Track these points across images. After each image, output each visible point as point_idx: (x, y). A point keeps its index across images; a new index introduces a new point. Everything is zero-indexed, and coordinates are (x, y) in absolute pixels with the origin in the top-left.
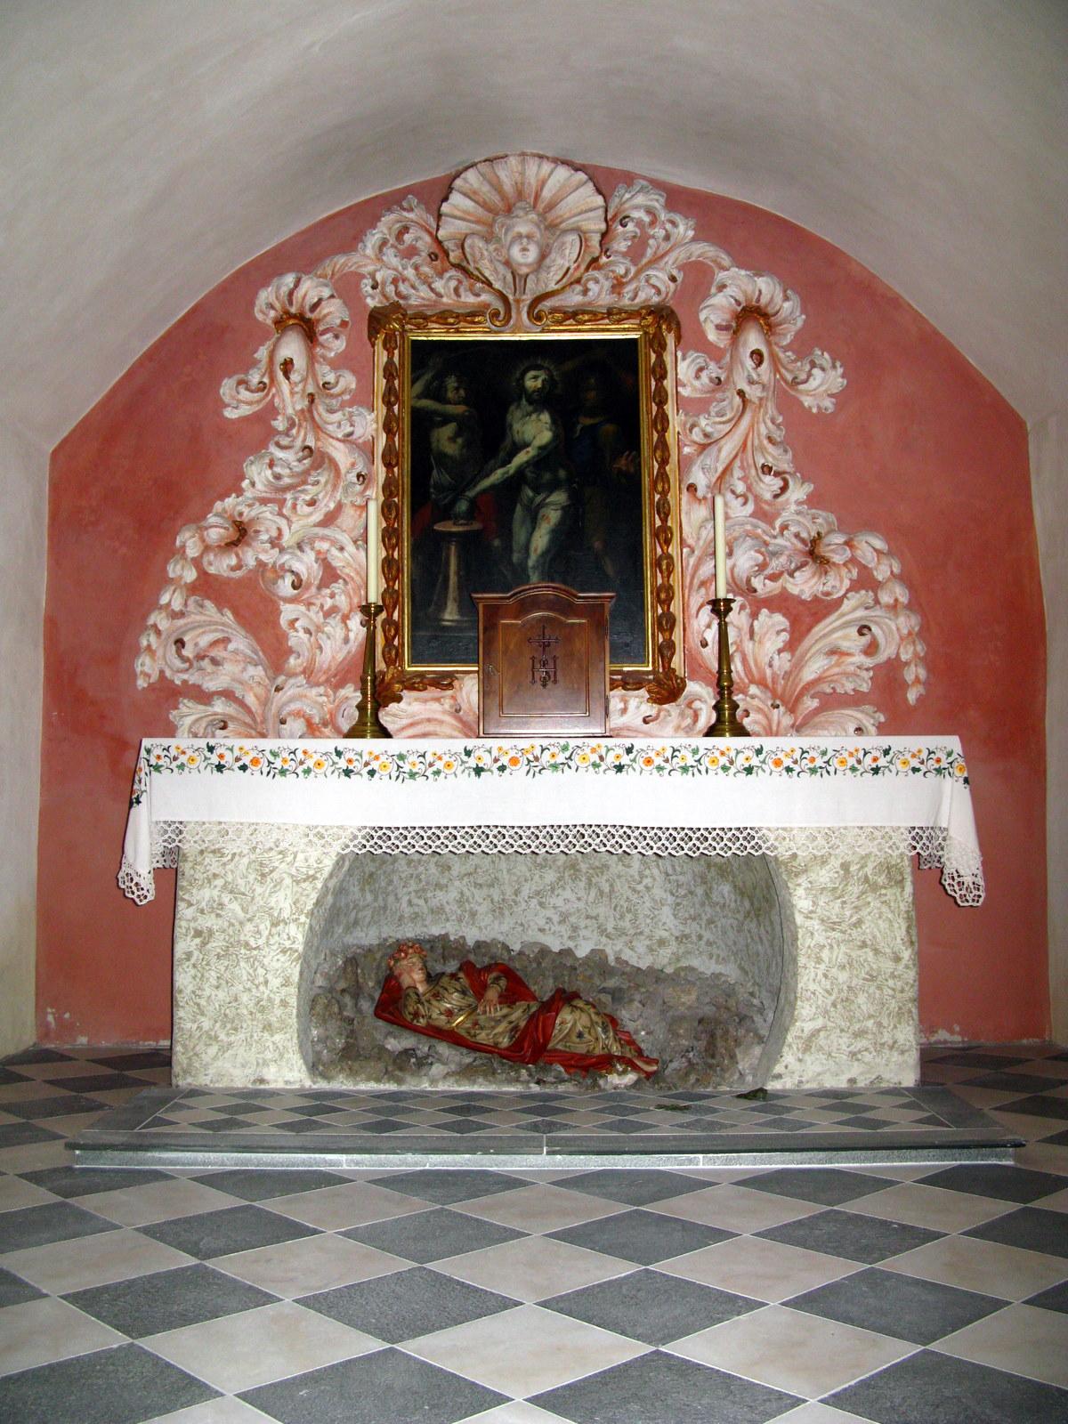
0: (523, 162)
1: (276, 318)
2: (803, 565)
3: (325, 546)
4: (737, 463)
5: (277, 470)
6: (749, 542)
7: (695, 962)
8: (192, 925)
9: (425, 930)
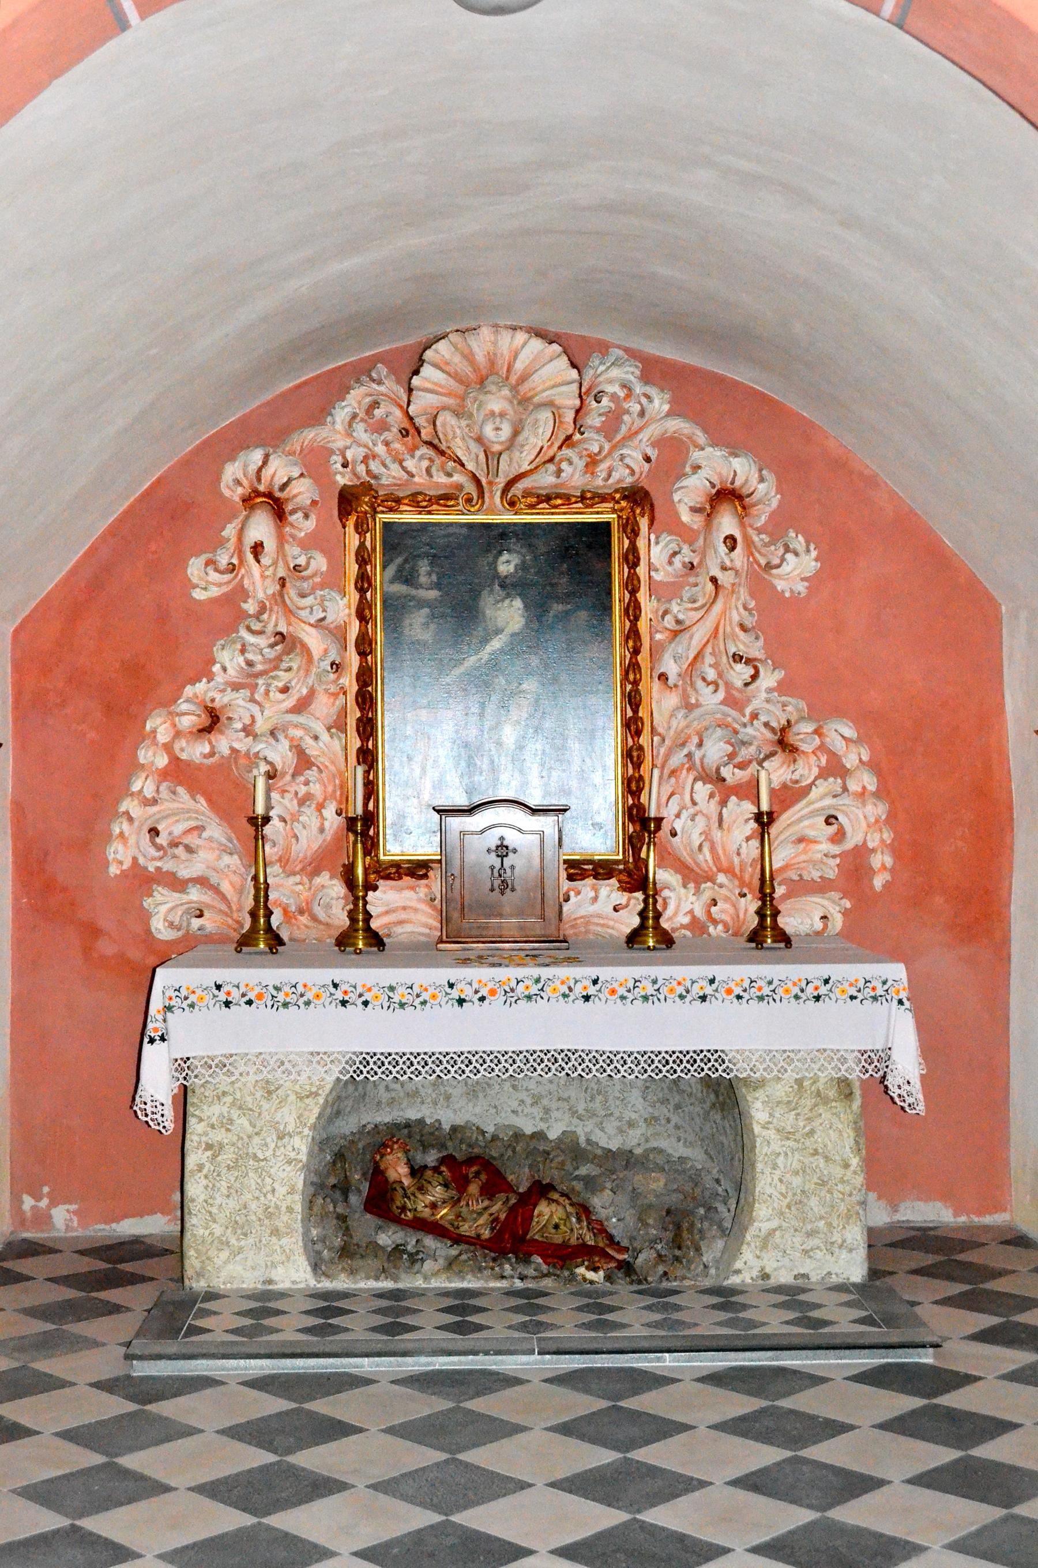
1: (244, 495)
2: (773, 754)
3: (298, 733)
4: (709, 649)
5: (250, 656)
6: (719, 732)
8: (204, 1139)
9: (401, 1113)
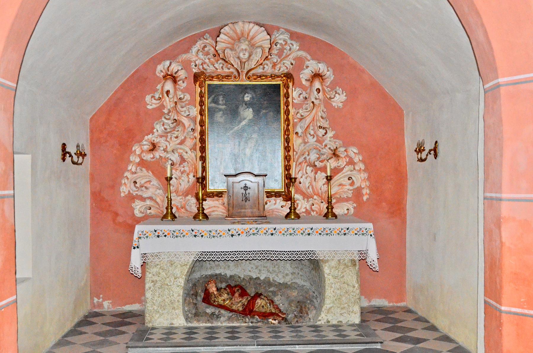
0: (243, 24)
3: (181, 151)
4: (311, 124)
5: (166, 127)
6: (315, 151)
7: (297, 281)
